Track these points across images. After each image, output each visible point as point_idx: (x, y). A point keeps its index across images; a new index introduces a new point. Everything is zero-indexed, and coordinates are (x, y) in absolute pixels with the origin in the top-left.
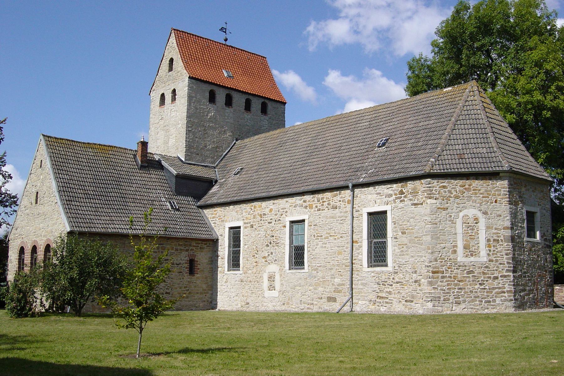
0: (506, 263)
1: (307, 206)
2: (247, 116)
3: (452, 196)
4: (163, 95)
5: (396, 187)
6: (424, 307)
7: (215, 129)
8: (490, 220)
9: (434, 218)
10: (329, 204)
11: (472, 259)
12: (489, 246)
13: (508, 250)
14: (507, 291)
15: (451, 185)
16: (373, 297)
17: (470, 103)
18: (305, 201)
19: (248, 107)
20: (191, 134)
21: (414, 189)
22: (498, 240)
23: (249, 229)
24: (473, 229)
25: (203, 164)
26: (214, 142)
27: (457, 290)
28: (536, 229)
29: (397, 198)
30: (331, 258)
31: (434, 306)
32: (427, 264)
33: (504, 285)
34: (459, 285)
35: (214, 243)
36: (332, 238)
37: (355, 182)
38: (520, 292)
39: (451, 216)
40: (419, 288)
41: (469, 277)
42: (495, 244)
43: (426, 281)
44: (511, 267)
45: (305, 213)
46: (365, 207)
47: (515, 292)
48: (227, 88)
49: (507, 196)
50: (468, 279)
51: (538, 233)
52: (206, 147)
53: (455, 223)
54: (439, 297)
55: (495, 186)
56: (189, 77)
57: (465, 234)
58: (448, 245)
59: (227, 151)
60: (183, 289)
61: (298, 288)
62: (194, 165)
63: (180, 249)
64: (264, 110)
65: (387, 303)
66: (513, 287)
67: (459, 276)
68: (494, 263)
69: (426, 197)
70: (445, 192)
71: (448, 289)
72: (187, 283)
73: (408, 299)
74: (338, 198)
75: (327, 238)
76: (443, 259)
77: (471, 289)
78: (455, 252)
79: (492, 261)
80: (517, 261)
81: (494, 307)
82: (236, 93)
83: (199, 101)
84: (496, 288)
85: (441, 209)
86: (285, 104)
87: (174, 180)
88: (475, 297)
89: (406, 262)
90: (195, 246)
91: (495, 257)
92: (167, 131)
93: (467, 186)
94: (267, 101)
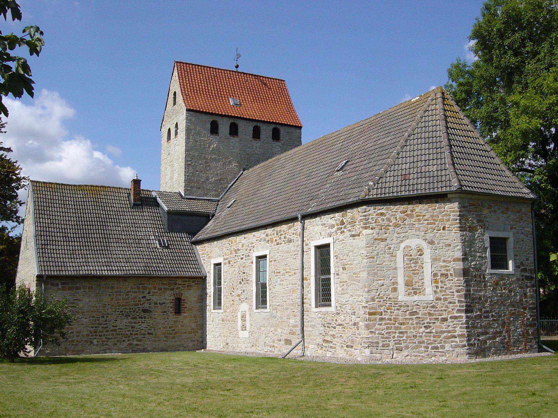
0: (457, 302)
1: (268, 241)
2: (257, 144)
3: (391, 224)
4: (169, 130)
5: (338, 216)
6: (363, 354)
7: (218, 161)
8: (437, 251)
9: (371, 251)
10: (285, 238)
11: (416, 298)
12: (436, 282)
13: (459, 286)
14: (459, 335)
15: (390, 212)
16: (320, 340)
17: (430, 113)
18: (267, 235)
19: (256, 134)
20: (190, 168)
21: (352, 218)
22: (447, 275)
23: (227, 265)
24: (416, 263)
25: (205, 198)
26: (217, 174)
27: (397, 334)
28: (508, 257)
29: (338, 229)
30: (287, 296)
31: (371, 353)
32: (364, 304)
33: (455, 328)
34: (400, 328)
35: (203, 279)
36: (287, 275)
37: (304, 212)
38: (478, 336)
39: (390, 248)
40: (357, 332)
41: (412, 319)
42: (443, 279)
43: (363, 324)
44: (463, 306)
45: (267, 248)
46: (313, 240)
47: (468, 336)
48: (231, 117)
49: (458, 221)
50: (411, 321)
51: (510, 263)
52: (208, 180)
53: (395, 256)
54: (377, 343)
55: (442, 210)
56: (187, 110)
57: (407, 268)
58: (387, 282)
59: (233, 182)
60: (168, 329)
61: (263, 329)
62: (195, 199)
63: (165, 289)
64: (276, 135)
65: (331, 347)
66: (466, 330)
67: (400, 318)
68: (442, 301)
69: (362, 227)
70: (383, 220)
71: (387, 333)
72: (173, 323)
73: (349, 344)
74: (292, 231)
75: (283, 275)
76: (382, 298)
77: (415, 334)
78: (395, 290)
79: (440, 299)
80: (474, 299)
81: (443, 354)
82: (242, 121)
83: (199, 134)
84: (445, 332)
85: (379, 240)
86: (301, 127)
87: (166, 216)
88: (420, 342)
89: (346, 301)
90: (180, 284)
91: (444, 295)
92: (172, 166)
93: (409, 212)
94: (278, 127)
